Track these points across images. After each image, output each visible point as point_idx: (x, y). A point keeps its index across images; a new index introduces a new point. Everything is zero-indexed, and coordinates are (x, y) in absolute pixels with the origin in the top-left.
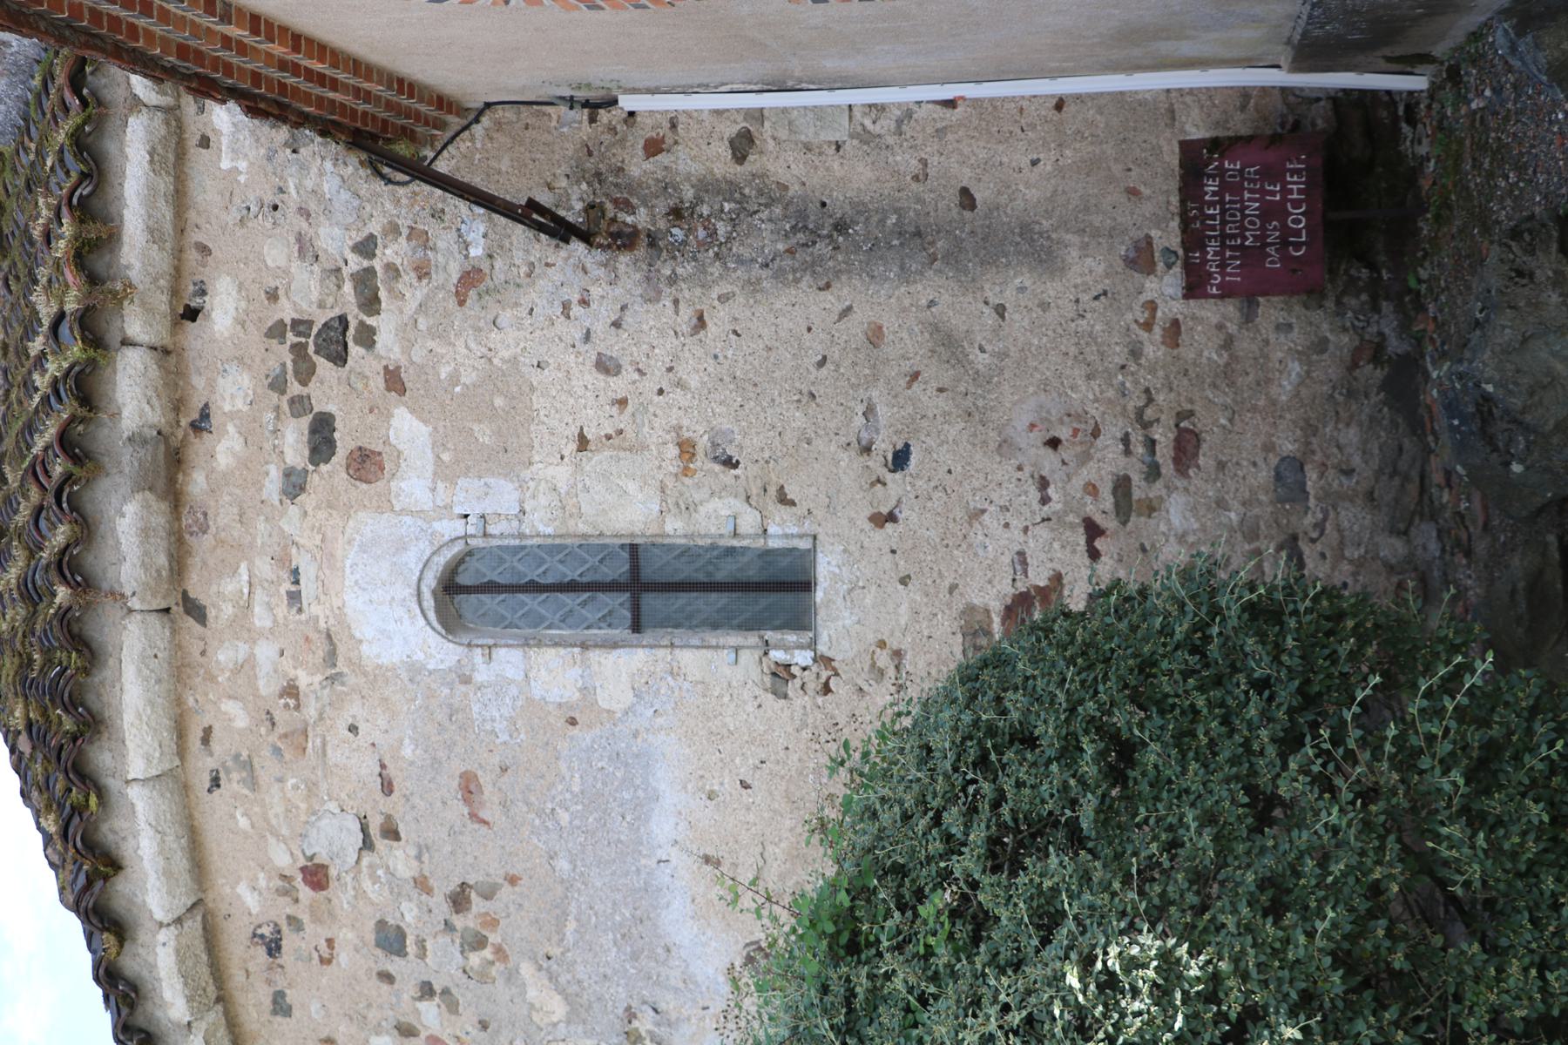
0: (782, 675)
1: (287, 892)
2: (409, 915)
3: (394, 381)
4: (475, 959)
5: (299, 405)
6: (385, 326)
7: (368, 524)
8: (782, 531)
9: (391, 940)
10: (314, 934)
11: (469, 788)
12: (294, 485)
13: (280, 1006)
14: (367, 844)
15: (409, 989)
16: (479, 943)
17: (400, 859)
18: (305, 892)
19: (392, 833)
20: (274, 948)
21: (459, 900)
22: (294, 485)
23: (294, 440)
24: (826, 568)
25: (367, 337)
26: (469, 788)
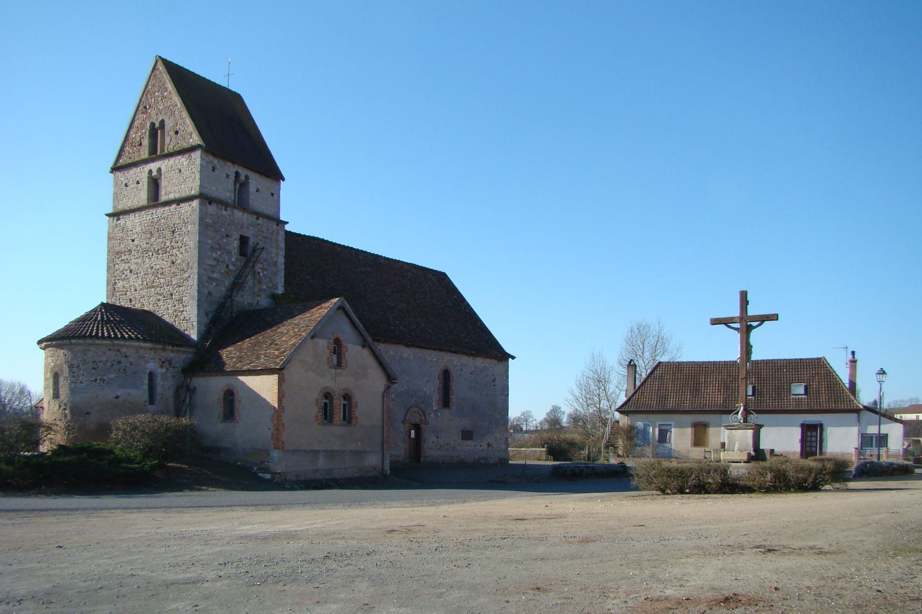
0: (146, 402)
1: (124, 354)
2: (122, 365)
3: (167, 369)
4: (117, 370)
5: (166, 360)
6: (171, 368)
7: (158, 366)
8: (157, 402)
9: (119, 362)
10: (119, 355)
11: (136, 373)
12: (160, 359)
13: (110, 350)
14: (130, 362)
15: (113, 363)
16: (119, 370)
17: (128, 365)
18: (125, 355)
19: (131, 364)
20: (118, 351)
21: (124, 370)
22: (160, 359)
23: (163, 360)
24: (155, 406)
25: (170, 367)
26: (136, 373)
